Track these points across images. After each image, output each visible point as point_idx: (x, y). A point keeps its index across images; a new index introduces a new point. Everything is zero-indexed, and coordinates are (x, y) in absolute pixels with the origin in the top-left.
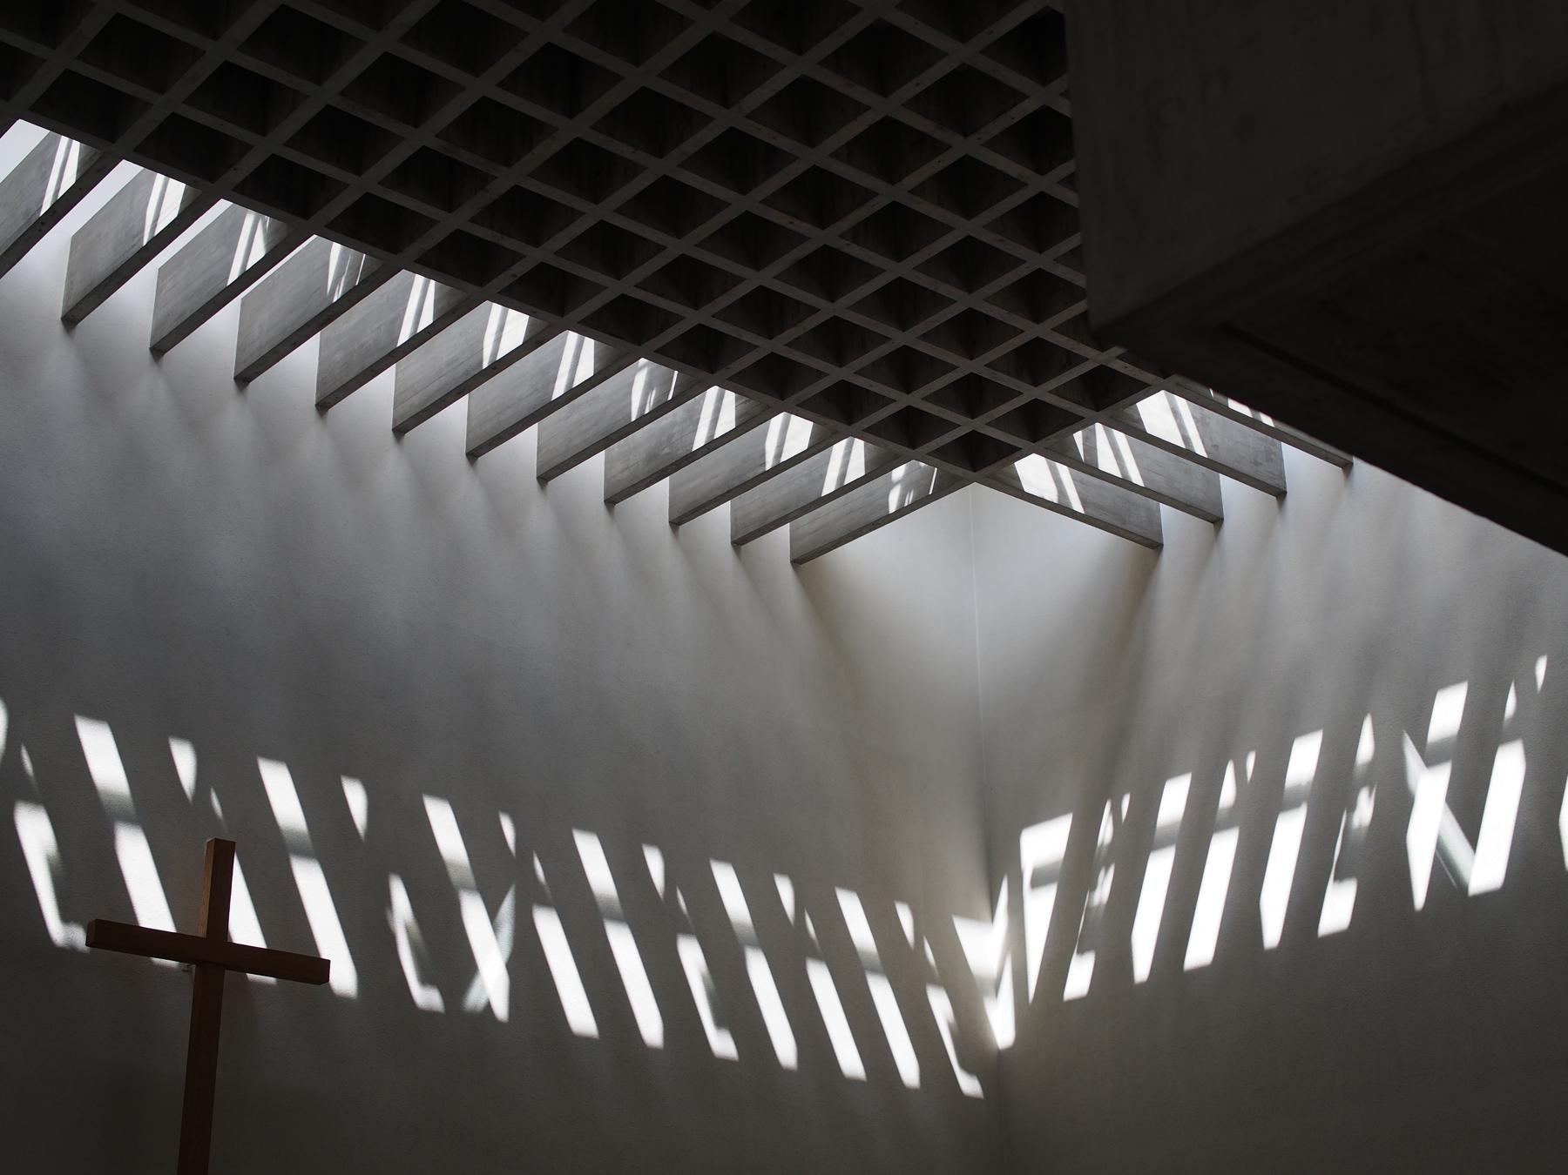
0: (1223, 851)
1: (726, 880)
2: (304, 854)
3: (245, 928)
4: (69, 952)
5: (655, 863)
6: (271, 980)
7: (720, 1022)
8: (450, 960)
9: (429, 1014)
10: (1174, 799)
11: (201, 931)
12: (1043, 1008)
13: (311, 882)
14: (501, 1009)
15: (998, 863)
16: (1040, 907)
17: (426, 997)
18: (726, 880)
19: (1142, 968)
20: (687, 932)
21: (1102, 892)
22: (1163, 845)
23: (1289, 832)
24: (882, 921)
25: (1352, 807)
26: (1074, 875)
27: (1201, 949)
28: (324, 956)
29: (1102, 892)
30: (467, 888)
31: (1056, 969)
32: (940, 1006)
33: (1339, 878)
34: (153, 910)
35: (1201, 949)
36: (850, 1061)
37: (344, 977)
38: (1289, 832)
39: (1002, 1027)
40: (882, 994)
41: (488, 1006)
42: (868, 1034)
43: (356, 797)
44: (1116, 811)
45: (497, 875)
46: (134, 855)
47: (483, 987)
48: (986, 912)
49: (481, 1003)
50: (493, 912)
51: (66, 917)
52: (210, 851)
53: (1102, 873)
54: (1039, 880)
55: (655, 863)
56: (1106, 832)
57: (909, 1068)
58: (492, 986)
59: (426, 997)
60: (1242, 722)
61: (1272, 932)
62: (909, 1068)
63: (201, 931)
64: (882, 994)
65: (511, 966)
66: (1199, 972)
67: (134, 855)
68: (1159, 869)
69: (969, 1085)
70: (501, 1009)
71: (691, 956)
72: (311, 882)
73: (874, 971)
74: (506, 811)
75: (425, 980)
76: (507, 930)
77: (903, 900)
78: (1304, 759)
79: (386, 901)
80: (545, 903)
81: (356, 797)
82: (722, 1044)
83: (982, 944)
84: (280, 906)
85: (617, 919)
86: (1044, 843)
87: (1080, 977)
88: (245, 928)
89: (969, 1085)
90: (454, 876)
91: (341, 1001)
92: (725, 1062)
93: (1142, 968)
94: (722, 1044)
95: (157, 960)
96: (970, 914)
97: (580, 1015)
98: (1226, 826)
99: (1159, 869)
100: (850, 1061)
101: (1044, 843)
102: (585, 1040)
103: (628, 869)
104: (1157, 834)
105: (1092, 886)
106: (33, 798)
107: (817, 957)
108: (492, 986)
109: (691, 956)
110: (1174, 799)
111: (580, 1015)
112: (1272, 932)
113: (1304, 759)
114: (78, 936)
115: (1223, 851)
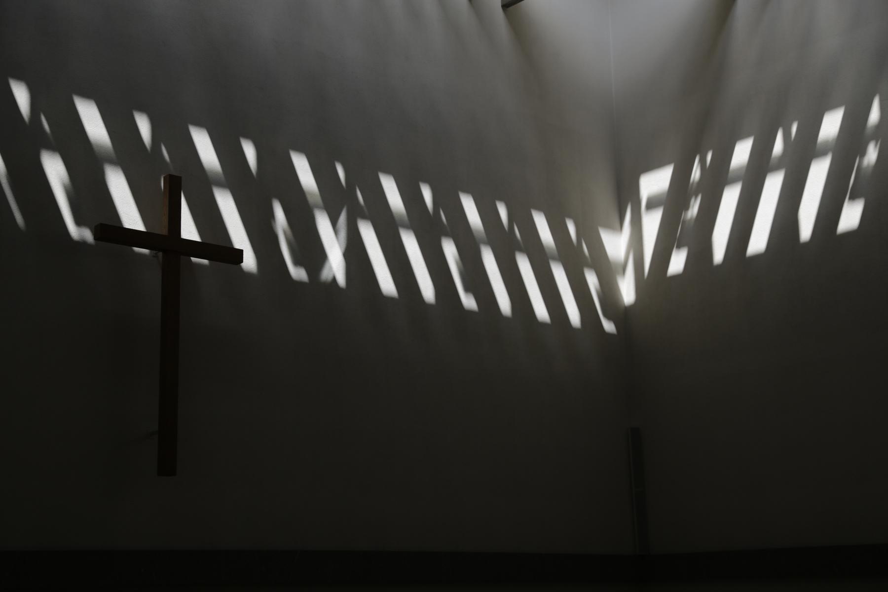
0: (773, 186)
1: (469, 205)
2: (221, 185)
3: (189, 231)
4: (82, 244)
5: (427, 194)
6: (205, 262)
7: (467, 289)
8: (311, 252)
9: (300, 284)
10: (742, 153)
11: (164, 231)
12: (654, 282)
13: (226, 203)
14: (341, 280)
15: (625, 195)
16: (652, 222)
17: (297, 273)
18: (469, 205)
19: (719, 254)
20: (447, 235)
21: (694, 210)
22: (733, 181)
23: (818, 174)
24: (558, 230)
25: (863, 153)
26: (674, 201)
27: (758, 241)
28: (237, 246)
29: (694, 210)
30: (318, 207)
31: (662, 256)
32: (592, 280)
33: (853, 198)
34: (131, 217)
35: (758, 242)
36: (541, 311)
37: (249, 262)
38: (818, 174)
39: (627, 291)
40: (559, 274)
41: (334, 279)
42: (552, 297)
43: (250, 151)
44: (703, 162)
45: (336, 200)
46: (118, 186)
47: (331, 268)
48: (617, 224)
49: (330, 278)
50: (334, 223)
51: (79, 221)
52: (169, 183)
53: (693, 200)
54: (652, 205)
55: (427, 194)
56: (696, 174)
57: (574, 315)
58: (336, 265)
59: (297, 273)
60: (789, 103)
61: (806, 231)
62: (574, 315)
63: (164, 231)
64: (559, 274)
65: (347, 255)
66: (757, 257)
67: (118, 186)
68: (730, 198)
69: (608, 326)
70: (341, 280)
71: (450, 250)
72: (226, 203)
73: (554, 259)
74: (339, 161)
75: (297, 262)
76: (343, 233)
77: (570, 217)
78: (831, 125)
79: (271, 215)
80: (364, 217)
81: (250, 151)
82: (468, 302)
83: (616, 244)
84: (209, 218)
85: (406, 227)
86: (655, 182)
87: (677, 263)
88: (189, 231)
89: (608, 326)
90: (310, 199)
91: (248, 275)
92: (470, 312)
93: (719, 254)
94: (468, 302)
95: (136, 249)
96: (609, 226)
97: (387, 284)
98: (775, 168)
99: (730, 198)
100: (541, 311)
101: (655, 182)
102: (390, 299)
103: (411, 197)
104: (818, 146)
105: (686, 206)
106: (53, 148)
107: (521, 250)
108: (336, 265)
109: (450, 250)
110: (742, 153)
111: (387, 284)
112: (806, 231)
113: (831, 125)
114: (87, 235)
115: (773, 186)
